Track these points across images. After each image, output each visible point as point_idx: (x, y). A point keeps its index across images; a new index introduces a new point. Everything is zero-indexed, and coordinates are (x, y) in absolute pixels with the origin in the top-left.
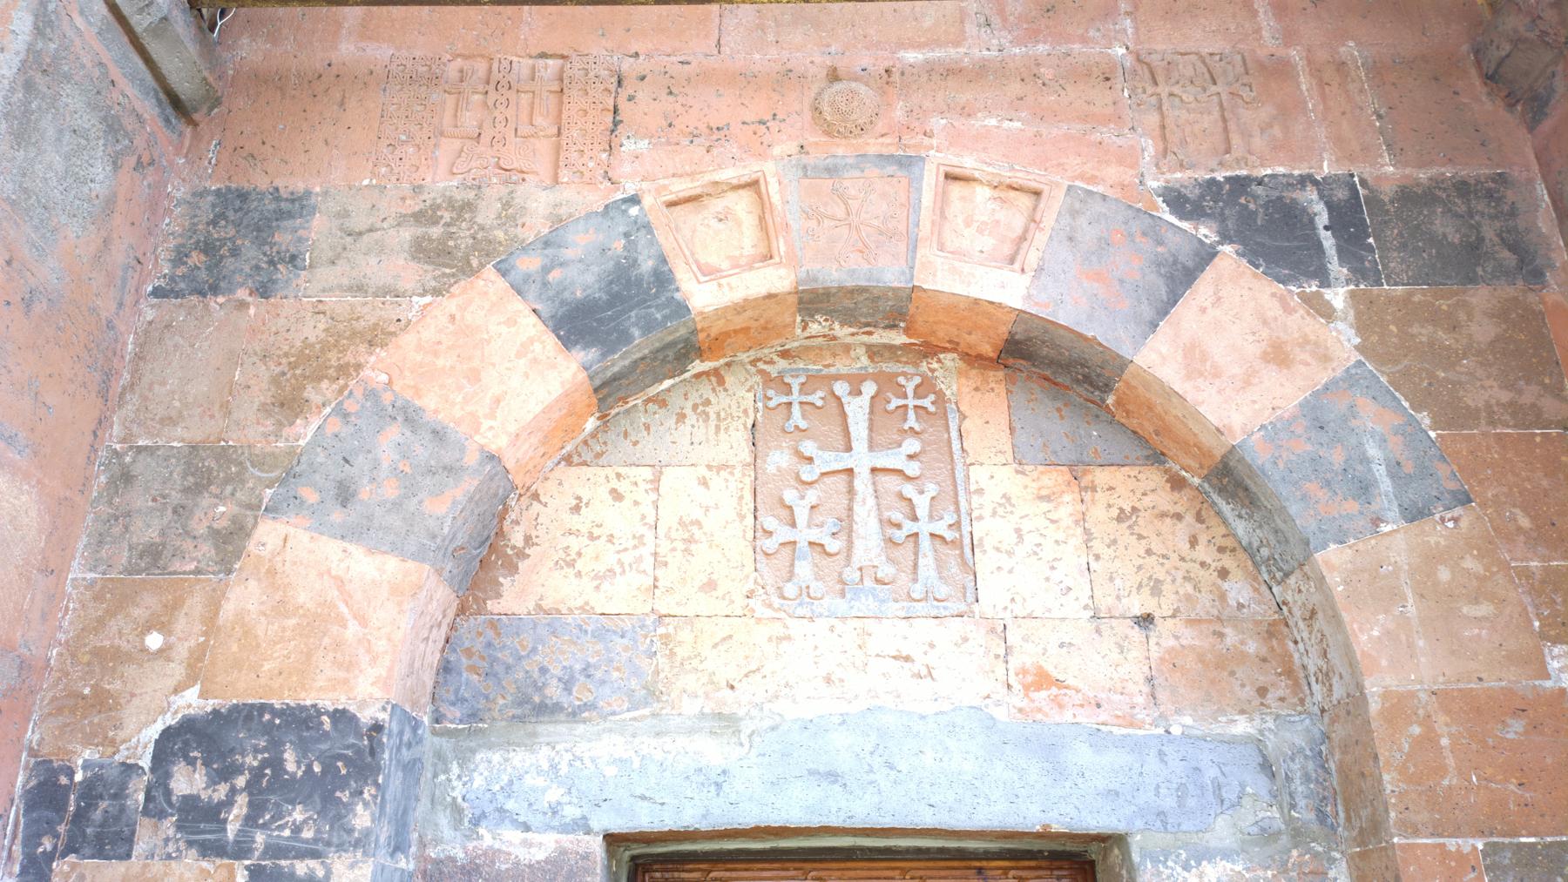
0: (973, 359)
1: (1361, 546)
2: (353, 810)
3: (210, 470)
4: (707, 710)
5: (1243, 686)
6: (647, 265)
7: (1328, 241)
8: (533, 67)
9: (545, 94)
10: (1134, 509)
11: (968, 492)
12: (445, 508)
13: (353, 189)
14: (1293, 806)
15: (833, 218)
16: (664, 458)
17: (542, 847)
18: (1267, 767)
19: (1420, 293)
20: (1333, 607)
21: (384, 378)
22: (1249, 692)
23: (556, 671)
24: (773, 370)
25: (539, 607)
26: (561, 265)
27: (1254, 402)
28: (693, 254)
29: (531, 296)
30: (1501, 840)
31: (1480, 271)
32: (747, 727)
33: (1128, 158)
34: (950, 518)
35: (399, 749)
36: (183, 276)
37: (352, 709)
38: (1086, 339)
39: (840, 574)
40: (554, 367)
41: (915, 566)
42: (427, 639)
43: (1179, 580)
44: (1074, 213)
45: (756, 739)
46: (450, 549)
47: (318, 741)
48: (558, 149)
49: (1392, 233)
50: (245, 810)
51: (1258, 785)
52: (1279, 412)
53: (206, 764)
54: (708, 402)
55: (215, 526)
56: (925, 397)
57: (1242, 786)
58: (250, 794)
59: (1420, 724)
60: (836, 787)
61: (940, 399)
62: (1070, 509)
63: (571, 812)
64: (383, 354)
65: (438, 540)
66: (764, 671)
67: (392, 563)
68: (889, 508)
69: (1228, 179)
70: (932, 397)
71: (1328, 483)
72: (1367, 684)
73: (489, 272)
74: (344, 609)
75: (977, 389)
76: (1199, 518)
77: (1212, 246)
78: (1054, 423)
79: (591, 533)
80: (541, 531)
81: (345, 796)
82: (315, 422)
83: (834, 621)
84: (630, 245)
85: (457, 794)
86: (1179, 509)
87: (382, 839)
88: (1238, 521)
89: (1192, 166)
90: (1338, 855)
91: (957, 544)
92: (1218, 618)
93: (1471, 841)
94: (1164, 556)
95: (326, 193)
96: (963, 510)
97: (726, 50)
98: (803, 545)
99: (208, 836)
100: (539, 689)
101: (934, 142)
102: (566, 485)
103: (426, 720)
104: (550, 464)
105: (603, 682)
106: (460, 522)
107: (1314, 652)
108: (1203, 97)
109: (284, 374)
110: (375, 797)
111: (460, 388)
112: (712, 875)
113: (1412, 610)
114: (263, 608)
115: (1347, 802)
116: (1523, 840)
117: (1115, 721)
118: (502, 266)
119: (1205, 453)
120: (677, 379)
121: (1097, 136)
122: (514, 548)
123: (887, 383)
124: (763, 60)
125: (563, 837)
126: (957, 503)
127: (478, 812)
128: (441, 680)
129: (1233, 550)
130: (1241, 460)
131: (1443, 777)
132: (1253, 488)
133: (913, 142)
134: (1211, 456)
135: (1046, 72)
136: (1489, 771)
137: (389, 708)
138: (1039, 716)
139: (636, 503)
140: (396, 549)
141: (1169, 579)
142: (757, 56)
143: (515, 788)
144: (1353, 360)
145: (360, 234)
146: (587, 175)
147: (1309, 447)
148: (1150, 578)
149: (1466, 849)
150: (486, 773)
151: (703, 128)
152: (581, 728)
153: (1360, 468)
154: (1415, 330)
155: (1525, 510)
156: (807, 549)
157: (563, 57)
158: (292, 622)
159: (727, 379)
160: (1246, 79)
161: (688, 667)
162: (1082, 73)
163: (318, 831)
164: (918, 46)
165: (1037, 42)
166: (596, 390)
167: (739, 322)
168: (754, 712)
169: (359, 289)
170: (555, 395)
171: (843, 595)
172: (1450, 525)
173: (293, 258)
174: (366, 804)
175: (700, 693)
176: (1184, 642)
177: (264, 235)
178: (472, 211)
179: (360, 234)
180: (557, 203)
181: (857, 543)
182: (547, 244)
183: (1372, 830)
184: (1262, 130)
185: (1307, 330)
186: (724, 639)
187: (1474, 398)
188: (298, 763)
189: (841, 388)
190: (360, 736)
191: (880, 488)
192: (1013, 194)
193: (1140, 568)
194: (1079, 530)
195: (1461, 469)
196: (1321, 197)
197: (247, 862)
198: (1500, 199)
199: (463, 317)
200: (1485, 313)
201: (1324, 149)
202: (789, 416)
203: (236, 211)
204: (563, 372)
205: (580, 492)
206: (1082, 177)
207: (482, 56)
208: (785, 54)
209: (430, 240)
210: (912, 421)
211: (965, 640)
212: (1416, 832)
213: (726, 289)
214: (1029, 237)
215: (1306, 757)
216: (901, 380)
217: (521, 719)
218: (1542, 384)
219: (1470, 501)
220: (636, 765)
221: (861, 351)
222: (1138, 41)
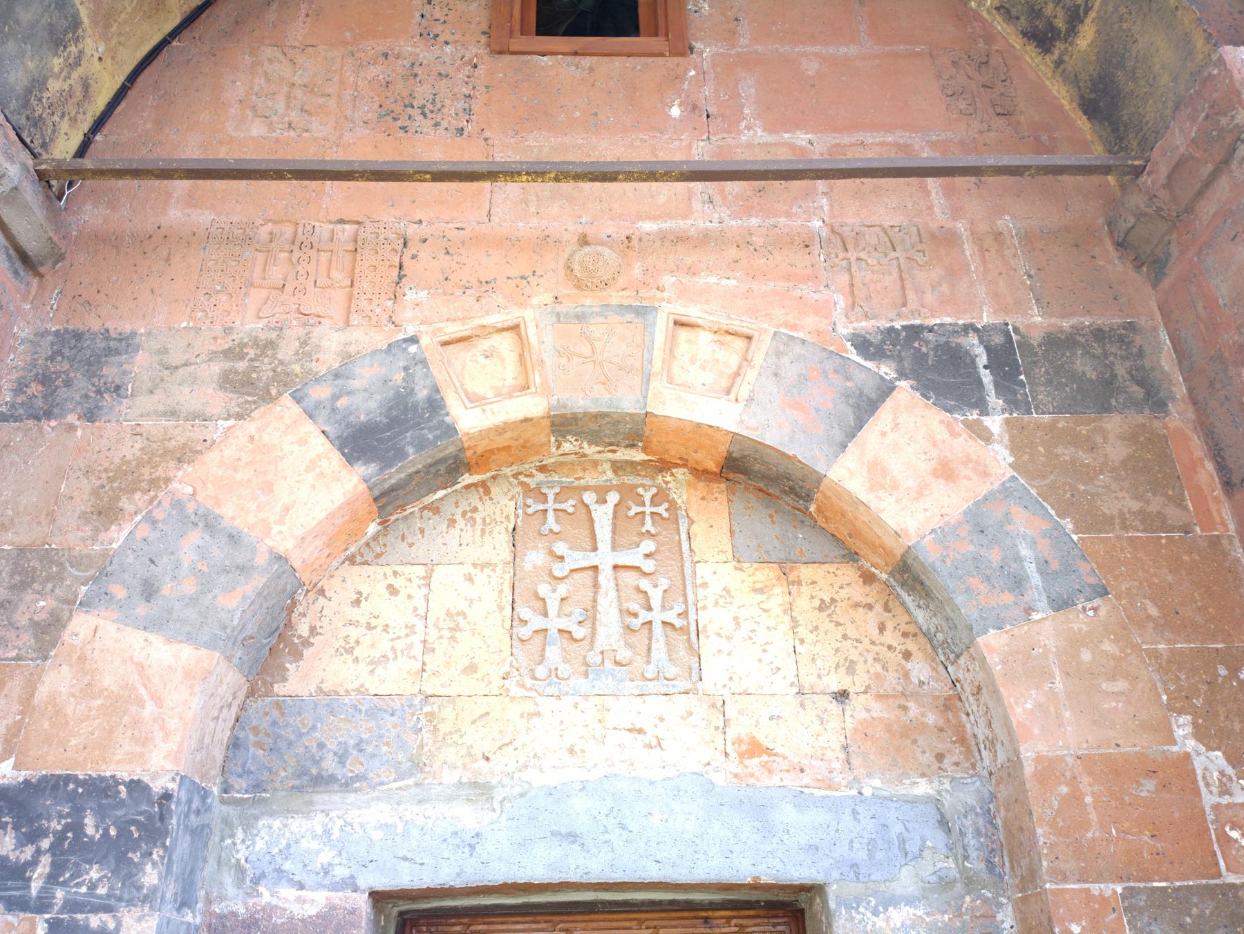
0: (700, 473)
1: (1016, 632)
2: (143, 870)
3: (34, 569)
4: (464, 780)
5: (924, 752)
6: (422, 394)
7: (987, 378)
8: (333, 231)
9: (341, 253)
10: (833, 600)
11: (694, 585)
12: (235, 602)
13: (174, 329)
14: (966, 858)
15: (580, 356)
17: (315, 902)
18: (943, 823)
19: (1064, 420)
20: (993, 684)
21: (189, 490)
22: (928, 758)
23: (332, 745)
24: (532, 482)
25: (320, 689)
26: (349, 393)
27: (926, 510)
28: (462, 385)
29: (321, 420)
30: (1137, 884)
31: (1113, 402)
32: (499, 794)
33: (823, 310)
34: (679, 608)
35: (187, 816)
36: (23, 404)
37: (146, 779)
38: (788, 457)
39: (585, 657)
40: (338, 479)
41: (649, 650)
42: (217, 718)
43: (870, 661)
44: (779, 354)
45: (507, 805)
46: (240, 638)
47: (116, 807)
48: (350, 298)
49: (1040, 371)
50: (48, 870)
51: (936, 839)
52: (947, 518)
53: (15, 828)
54: (475, 510)
55: (36, 618)
56: (660, 505)
57: (923, 840)
58: (53, 855)
59: (1067, 785)
60: (576, 847)
61: (673, 507)
62: (779, 600)
63: (341, 872)
64: (190, 469)
65: (229, 631)
66: (516, 744)
68: (628, 600)
69: (904, 327)
70: (666, 505)
71: (988, 578)
72: (1022, 749)
73: (286, 400)
74: (142, 691)
75: (703, 498)
76: (887, 608)
78: (764, 526)
80: (325, 622)
81: (135, 857)
82: (127, 528)
84: (409, 377)
85: (240, 856)
86: (870, 600)
87: (168, 896)
89: (875, 317)
90: (1004, 900)
91: (684, 630)
92: (903, 694)
93: (1112, 886)
94: (858, 641)
95: (149, 334)
96: (690, 601)
97: (495, 219)
98: (553, 632)
99: (14, 893)
100: (317, 763)
101: (666, 295)
102: (349, 582)
103: (215, 790)
104: (335, 564)
105: (373, 756)
106: (249, 615)
107: (982, 722)
108: (884, 261)
109: (103, 486)
110: (162, 858)
112: (473, 928)
113: (1059, 686)
114: (73, 690)
115: (1011, 853)
116: (1156, 884)
117: (816, 784)
118: (297, 394)
119: (888, 553)
120: (449, 490)
121: (798, 293)
122: (300, 637)
123: (629, 493)
124: (526, 227)
125: (332, 894)
126: (685, 595)
127: (258, 873)
128: (230, 754)
129: (915, 635)
130: (916, 558)
131: (1087, 830)
132: (927, 582)
133: (648, 295)
134: (893, 555)
135: (758, 241)
136: (1126, 825)
137: (178, 779)
138: (752, 781)
139: (410, 597)
140: (190, 639)
141: (862, 660)
142: (521, 224)
143: (292, 850)
144: (1008, 476)
145: (177, 368)
146: (374, 319)
147: (972, 548)
148: (846, 659)
149: (1108, 893)
150: (267, 838)
151: (474, 281)
152: (352, 797)
153: (1014, 565)
154: (1060, 450)
155: (1153, 600)
156: (557, 635)
157: (358, 223)
158: (99, 702)
161: (449, 741)
163: (111, 888)
164: (655, 218)
165: (751, 216)
166: (376, 500)
167: (501, 442)
168: (506, 781)
169: (173, 414)
170: (337, 504)
171: (586, 675)
172: (1091, 613)
173: (118, 388)
174: (154, 864)
175: (459, 764)
176: (874, 715)
177: (94, 369)
178: (273, 349)
179: (177, 368)
181: (600, 629)
182: (337, 376)
183: (1030, 878)
184: (933, 288)
186: (482, 716)
187: (1109, 507)
188: (97, 827)
189: (589, 498)
190: (152, 804)
191: (620, 582)
192: (729, 338)
193: (837, 650)
194: (787, 618)
195: (1099, 567)
196: (981, 342)
197: (47, 916)
198: (1130, 343)
200: (1119, 437)
201: (984, 303)
202: (544, 521)
203: (71, 349)
204: (347, 483)
206: (785, 325)
208: (544, 224)
209: (236, 372)
210: (648, 526)
211: (690, 714)
212: (1065, 879)
214: (742, 372)
215: (977, 814)
216: (640, 491)
217: (299, 789)
218: (1166, 495)
219: (1107, 594)
220: (400, 830)
221: (607, 466)
222: (832, 216)
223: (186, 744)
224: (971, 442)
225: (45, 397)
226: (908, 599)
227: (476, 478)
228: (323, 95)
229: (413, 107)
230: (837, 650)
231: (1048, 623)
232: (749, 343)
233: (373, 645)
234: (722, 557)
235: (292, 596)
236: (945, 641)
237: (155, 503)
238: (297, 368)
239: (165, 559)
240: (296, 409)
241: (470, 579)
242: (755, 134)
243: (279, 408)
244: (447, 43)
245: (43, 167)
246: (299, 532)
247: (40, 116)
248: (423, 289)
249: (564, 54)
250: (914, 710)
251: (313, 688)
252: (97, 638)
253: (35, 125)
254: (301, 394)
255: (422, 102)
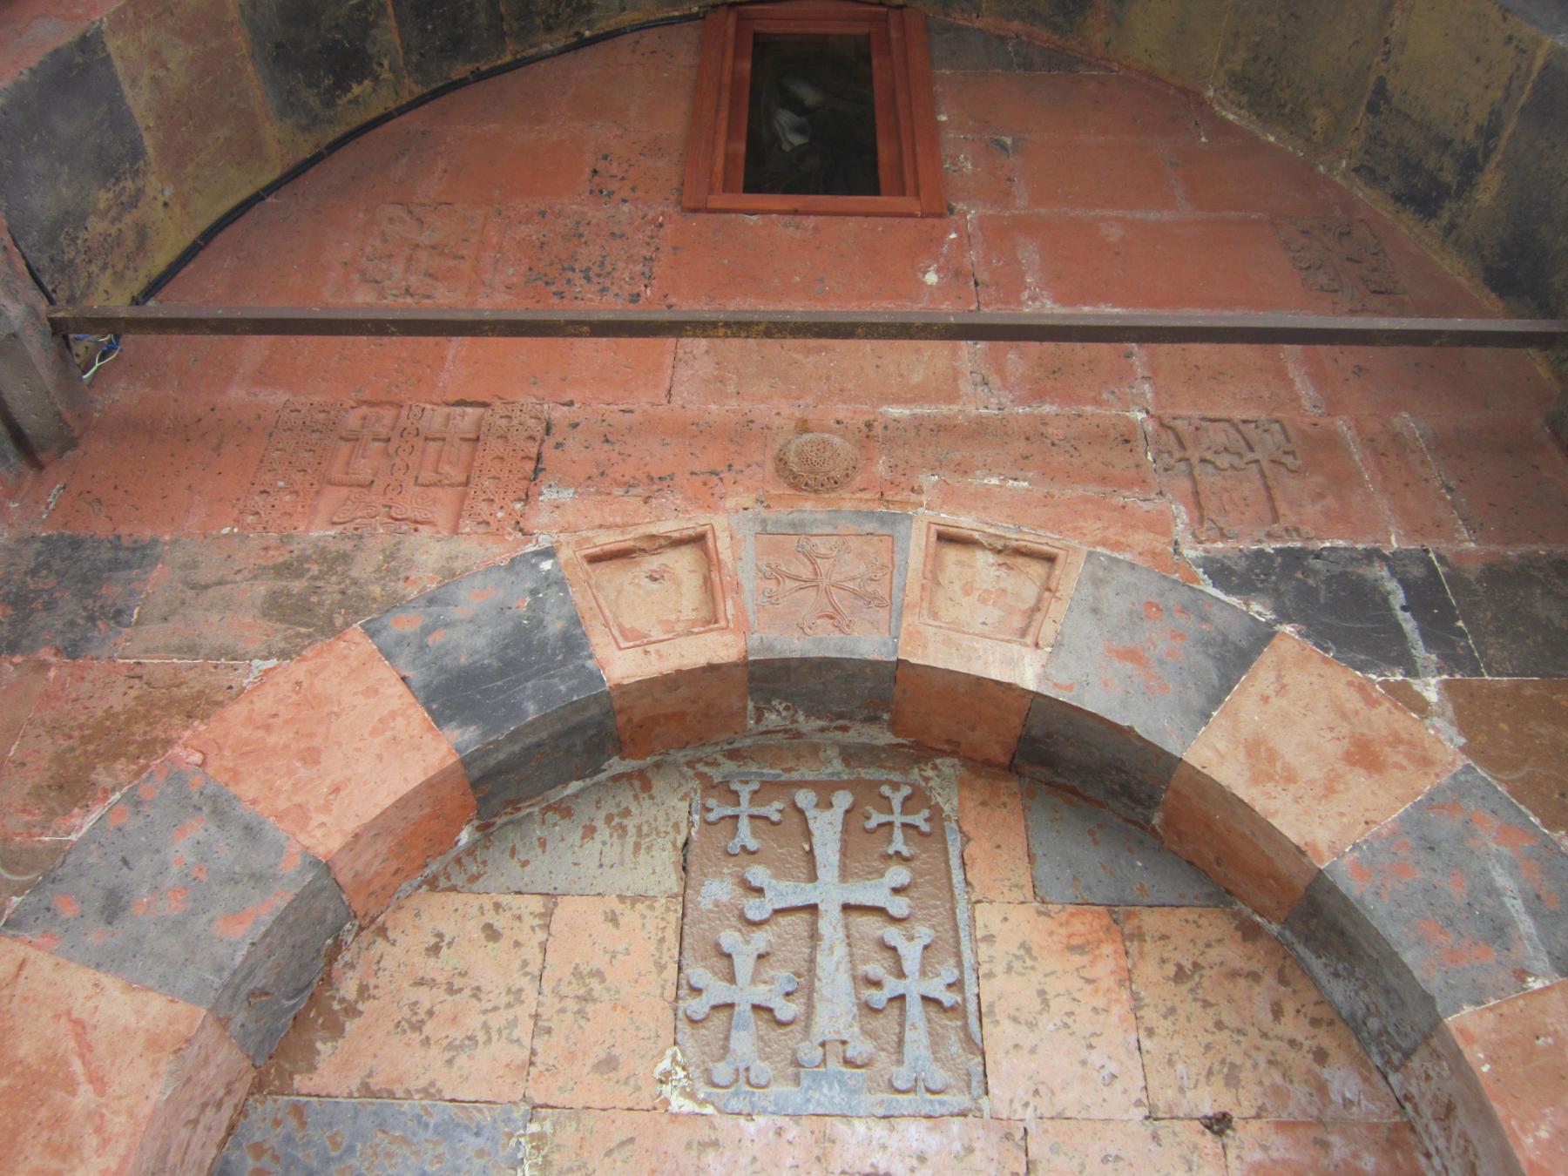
0: (980, 767)
7: (1408, 623)
9: (457, 442)
10: (1196, 965)
11: (974, 940)
12: (238, 931)
16: (561, 884)
21: (198, 758)
24: (716, 775)
27: (1342, 814)
28: (616, 617)
29: (401, 662)
33: (1158, 524)
34: (950, 975)
39: (794, 1052)
41: (900, 1042)
42: (196, 1122)
43: (1263, 1065)
46: (245, 989)
56: (916, 812)
61: (937, 815)
64: (202, 728)
67: (157, 1004)
68: (865, 961)
70: (926, 813)
74: (77, 1066)
75: (984, 804)
76: (1283, 980)
77: (1268, 624)
79: (450, 984)
80: (383, 978)
83: (781, 1121)
84: (537, 605)
86: (1255, 966)
88: (1334, 982)
95: (175, 542)
96: (967, 965)
97: (677, 401)
98: (743, 1008)
101: (924, 499)
111: (291, 772)
122: (342, 1000)
126: (958, 955)
129: (1331, 1023)
132: (1351, 930)
133: (898, 498)
139: (517, 944)
140: (166, 985)
141: (1249, 1064)
144: (1459, 766)
145: (206, 587)
146: (494, 525)
153: (1489, 902)
159: (654, 782)
160: (1288, 447)
162: (1099, 436)
164: (897, 400)
169: (191, 650)
171: (797, 1080)
173: (119, 613)
176: (1276, 1155)
177: (91, 587)
178: (346, 563)
179: (206, 587)
180: (461, 568)
182: (432, 601)
185: (1397, 726)
186: (623, 1144)
191: (853, 932)
192: (1020, 561)
193: (1208, 1047)
194: (1125, 995)
196: (1393, 573)
199: (312, 684)
205: (441, 927)
206: (1104, 543)
207: (391, 403)
208: (746, 406)
209: (289, 595)
210: (898, 843)
213: (653, 656)
216: (885, 790)
221: (833, 752)
223: (132, 1160)
224: (1397, 714)
225: (13, 624)
226: (1317, 965)
227: (629, 765)
228: (456, 257)
229: (573, 270)
230: (1208, 1047)
231: (1555, 995)
232: (1051, 568)
233: (454, 1020)
234: (1017, 895)
235: (336, 931)
236: (1383, 1031)
237: (144, 776)
238: (376, 590)
239: (145, 859)
240: (369, 646)
241: (613, 919)
242: (1043, 306)
243: (342, 644)
244: (625, 201)
245: (60, 315)
246: (351, 826)
247: (71, 261)
248: (568, 487)
249: (781, 213)
250: (1340, 1149)
251: (355, 1084)
252: (22, 980)
253: (62, 270)
254: (377, 625)
255: (586, 265)
